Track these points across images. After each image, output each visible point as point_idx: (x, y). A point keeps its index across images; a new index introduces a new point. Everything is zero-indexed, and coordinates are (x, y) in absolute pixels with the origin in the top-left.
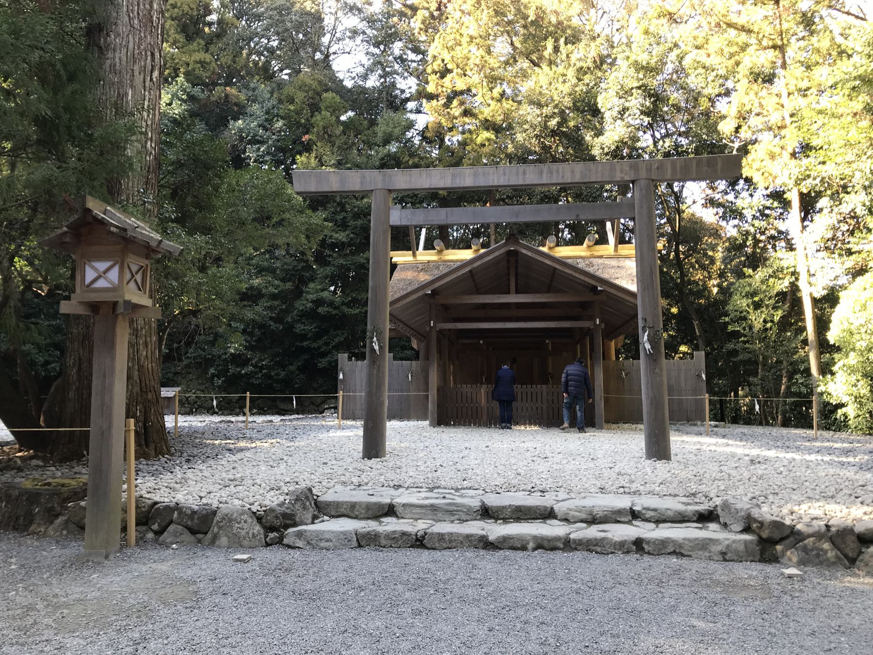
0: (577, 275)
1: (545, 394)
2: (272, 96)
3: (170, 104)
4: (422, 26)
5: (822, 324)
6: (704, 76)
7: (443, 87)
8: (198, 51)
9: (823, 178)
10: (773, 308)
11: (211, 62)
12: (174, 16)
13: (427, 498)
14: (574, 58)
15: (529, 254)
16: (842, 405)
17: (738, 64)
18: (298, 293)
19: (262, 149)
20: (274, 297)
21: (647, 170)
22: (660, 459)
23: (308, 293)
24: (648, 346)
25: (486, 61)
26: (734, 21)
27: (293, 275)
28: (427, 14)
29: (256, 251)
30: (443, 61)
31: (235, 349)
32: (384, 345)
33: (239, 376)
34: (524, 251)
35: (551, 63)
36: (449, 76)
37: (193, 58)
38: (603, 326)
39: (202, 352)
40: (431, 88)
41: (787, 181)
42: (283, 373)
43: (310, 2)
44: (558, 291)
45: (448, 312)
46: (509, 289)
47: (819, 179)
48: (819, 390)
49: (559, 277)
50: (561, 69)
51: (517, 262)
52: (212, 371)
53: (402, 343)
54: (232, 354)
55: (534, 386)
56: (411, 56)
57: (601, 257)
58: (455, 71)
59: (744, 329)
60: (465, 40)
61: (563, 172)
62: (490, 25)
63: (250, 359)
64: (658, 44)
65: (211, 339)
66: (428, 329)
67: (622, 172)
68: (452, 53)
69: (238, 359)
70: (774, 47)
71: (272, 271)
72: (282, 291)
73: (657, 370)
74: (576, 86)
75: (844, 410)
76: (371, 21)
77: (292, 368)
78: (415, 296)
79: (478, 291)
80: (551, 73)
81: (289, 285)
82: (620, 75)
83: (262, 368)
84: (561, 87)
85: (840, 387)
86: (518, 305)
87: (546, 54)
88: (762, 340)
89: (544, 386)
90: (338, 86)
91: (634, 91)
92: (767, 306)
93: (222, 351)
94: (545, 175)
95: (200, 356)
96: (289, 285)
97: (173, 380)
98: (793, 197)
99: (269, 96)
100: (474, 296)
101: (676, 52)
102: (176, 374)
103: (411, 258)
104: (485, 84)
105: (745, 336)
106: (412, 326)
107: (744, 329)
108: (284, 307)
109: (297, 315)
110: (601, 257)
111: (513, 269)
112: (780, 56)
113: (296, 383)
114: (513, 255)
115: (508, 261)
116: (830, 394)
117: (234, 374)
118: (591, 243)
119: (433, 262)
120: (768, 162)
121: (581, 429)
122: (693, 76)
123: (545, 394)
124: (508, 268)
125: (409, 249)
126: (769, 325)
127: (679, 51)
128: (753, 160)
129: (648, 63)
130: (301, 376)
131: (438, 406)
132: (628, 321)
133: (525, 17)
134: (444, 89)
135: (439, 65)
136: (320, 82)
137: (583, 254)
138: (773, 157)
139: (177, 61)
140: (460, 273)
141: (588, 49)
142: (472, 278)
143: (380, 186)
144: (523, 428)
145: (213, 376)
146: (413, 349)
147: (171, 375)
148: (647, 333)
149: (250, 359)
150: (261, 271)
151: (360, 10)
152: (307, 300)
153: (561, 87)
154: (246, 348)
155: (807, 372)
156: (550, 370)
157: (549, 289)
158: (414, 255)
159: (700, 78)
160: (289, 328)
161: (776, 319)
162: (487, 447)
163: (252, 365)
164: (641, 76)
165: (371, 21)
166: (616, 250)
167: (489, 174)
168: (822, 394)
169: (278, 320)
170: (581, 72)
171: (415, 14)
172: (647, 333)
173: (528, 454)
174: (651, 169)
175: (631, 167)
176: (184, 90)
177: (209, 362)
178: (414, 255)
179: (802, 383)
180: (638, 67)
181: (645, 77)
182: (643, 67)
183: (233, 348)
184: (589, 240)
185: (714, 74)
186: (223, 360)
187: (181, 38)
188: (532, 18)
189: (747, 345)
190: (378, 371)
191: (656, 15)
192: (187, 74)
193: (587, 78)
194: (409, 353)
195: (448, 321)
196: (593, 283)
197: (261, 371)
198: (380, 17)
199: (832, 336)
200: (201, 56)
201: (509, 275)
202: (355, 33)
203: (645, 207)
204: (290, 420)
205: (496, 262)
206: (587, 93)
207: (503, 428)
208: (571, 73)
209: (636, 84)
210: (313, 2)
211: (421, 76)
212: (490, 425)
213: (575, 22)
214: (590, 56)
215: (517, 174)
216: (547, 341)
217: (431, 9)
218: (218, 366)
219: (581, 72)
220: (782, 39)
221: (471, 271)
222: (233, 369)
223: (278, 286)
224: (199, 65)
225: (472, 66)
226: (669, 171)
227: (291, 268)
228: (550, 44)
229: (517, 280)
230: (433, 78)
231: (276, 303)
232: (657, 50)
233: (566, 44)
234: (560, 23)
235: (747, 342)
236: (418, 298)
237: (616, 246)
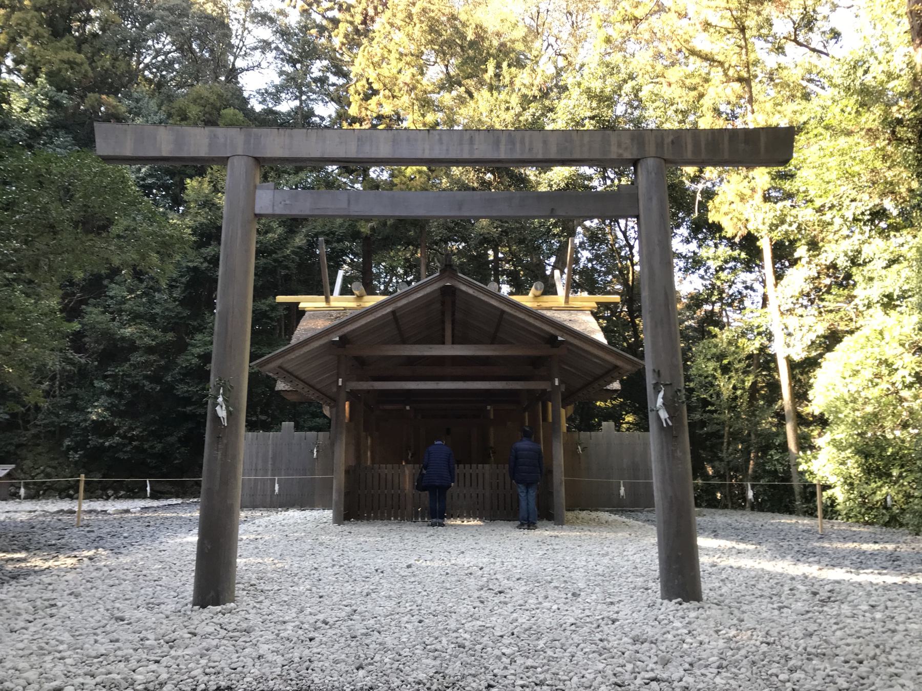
0: (531, 320)
2: (160, 109)
3: (26, 110)
4: (344, 41)
5: (801, 395)
6: (662, 109)
7: (367, 109)
8: (68, 49)
9: (799, 224)
10: (743, 373)
11: (82, 64)
12: (38, 5)
14: (518, 83)
15: (470, 291)
16: (826, 487)
17: (701, 96)
18: (181, 347)
19: (143, 170)
20: (150, 350)
22: (687, 600)
23: (194, 346)
24: (664, 415)
25: (418, 81)
26: (698, 49)
27: (176, 323)
28: (350, 29)
29: (131, 294)
30: (368, 80)
31: (98, 414)
32: (237, 410)
33: (101, 449)
34: (464, 288)
35: (491, 88)
36: (375, 99)
37: (59, 57)
39: (55, 419)
40: (353, 111)
41: (761, 227)
42: (159, 446)
43: (211, 4)
44: (502, 342)
45: (363, 367)
46: (444, 336)
47: (795, 226)
48: (800, 469)
49: (505, 324)
50: (503, 96)
51: (454, 302)
52: (67, 442)
53: (313, 409)
54: (93, 421)
55: (474, 466)
56: (333, 79)
57: (550, 309)
58: (382, 92)
59: (711, 396)
60: (394, 56)
62: (423, 41)
63: (118, 428)
64: (612, 74)
65: (69, 402)
66: (335, 390)
67: (619, 146)
68: (378, 71)
69: (100, 428)
70: (740, 80)
71: (152, 319)
72: (162, 344)
73: (679, 454)
74: (519, 115)
75: (829, 492)
76: (285, 33)
77: (172, 439)
78: (316, 344)
79: (404, 341)
80: (492, 101)
81: (170, 336)
82: (571, 103)
83: (132, 439)
84: (503, 115)
85: (827, 464)
87: (487, 77)
88: (732, 409)
89: (487, 466)
91: (586, 121)
92: (737, 370)
93: (81, 418)
94: (503, 147)
95: (53, 423)
96: (170, 336)
97: (15, 454)
98: (765, 245)
99: (156, 108)
100: (398, 346)
101: (631, 83)
102: (19, 446)
103: (324, 304)
104: (416, 107)
105: (713, 405)
106: (318, 387)
107: (711, 396)
108: (162, 363)
109: (179, 373)
110: (550, 309)
111: (448, 312)
112: (746, 89)
113: (176, 458)
114: (448, 293)
115: (443, 303)
116: (812, 473)
117: (95, 447)
118: (539, 293)
119: (350, 309)
120: (738, 205)
121: (528, 523)
122: (651, 109)
124: (443, 313)
125: (320, 293)
126: (739, 392)
127: (634, 83)
128: (721, 203)
129: (602, 92)
130: (183, 449)
131: (347, 494)
133: (463, 37)
134: (369, 113)
135: (364, 86)
136: (220, 96)
138: (742, 198)
139: (38, 58)
140: (379, 314)
141: (534, 76)
142: (395, 324)
144: (459, 522)
145: (69, 448)
146: (325, 416)
147: (12, 448)
148: (661, 394)
149: (118, 428)
150: (136, 317)
151: (272, 20)
152: (193, 355)
153: (503, 115)
154: (113, 414)
155: (784, 447)
156: (492, 444)
157: (493, 340)
158: (327, 300)
159: (659, 113)
160: (169, 389)
161: (748, 384)
162: (409, 566)
163: (119, 435)
164: (594, 104)
165: (285, 33)
166: (567, 301)
168: (802, 473)
169: (155, 379)
170: (526, 101)
171: (337, 27)
172: (661, 394)
173: (471, 582)
175: (632, 140)
176: (46, 95)
177: (65, 431)
178: (327, 300)
179: (777, 460)
180: (590, 94)
181: (598, 107)
182: (596, 96)
183: (95, 413)
184: (536, 288)
185: (674, 107)
186: (83, 429)
187: (45, 31)
188: (470, 36)
189: (715, 415)
190: (225, 454)
191: (620, 19)
192: (50, 76)
193: (533, 108)
194: (319, 421)
195: (360, 379)
196: (552, 331)
197: (130, 443)
198: (297, 31)
199: (816, 405)
200: (71, 55)
201: (443, 322)
202: (265, 46)
203: (655, 201)
204: (156, 509)
205: (427, 302)
206: (533, 123)
207: (433, 525)
208: (515, 100)
209: (589, 114)
210: (215, 4)
211: (341, 101)
212: (417, 518)
213: (519, 46)
214: (536, 83)
216: (489, 408)
217: (356, 23)
218: (76, 436)
219: (526, 101)
220: (748, 71)
221: (393, 312)
222: (94, 441)
223: (156, 337)
224: (66, 66)
225: (401, 85)
226: (690, 147)
227: (173, 315)
228: (491, 66)
229: (453, 330)
230: (355, 99)
231: (153, 358)
232: (611, 82)
233: (509, 66)
234: (503, 45)
235: (715, 411)
236: (321, 346)
237: (567, 296)
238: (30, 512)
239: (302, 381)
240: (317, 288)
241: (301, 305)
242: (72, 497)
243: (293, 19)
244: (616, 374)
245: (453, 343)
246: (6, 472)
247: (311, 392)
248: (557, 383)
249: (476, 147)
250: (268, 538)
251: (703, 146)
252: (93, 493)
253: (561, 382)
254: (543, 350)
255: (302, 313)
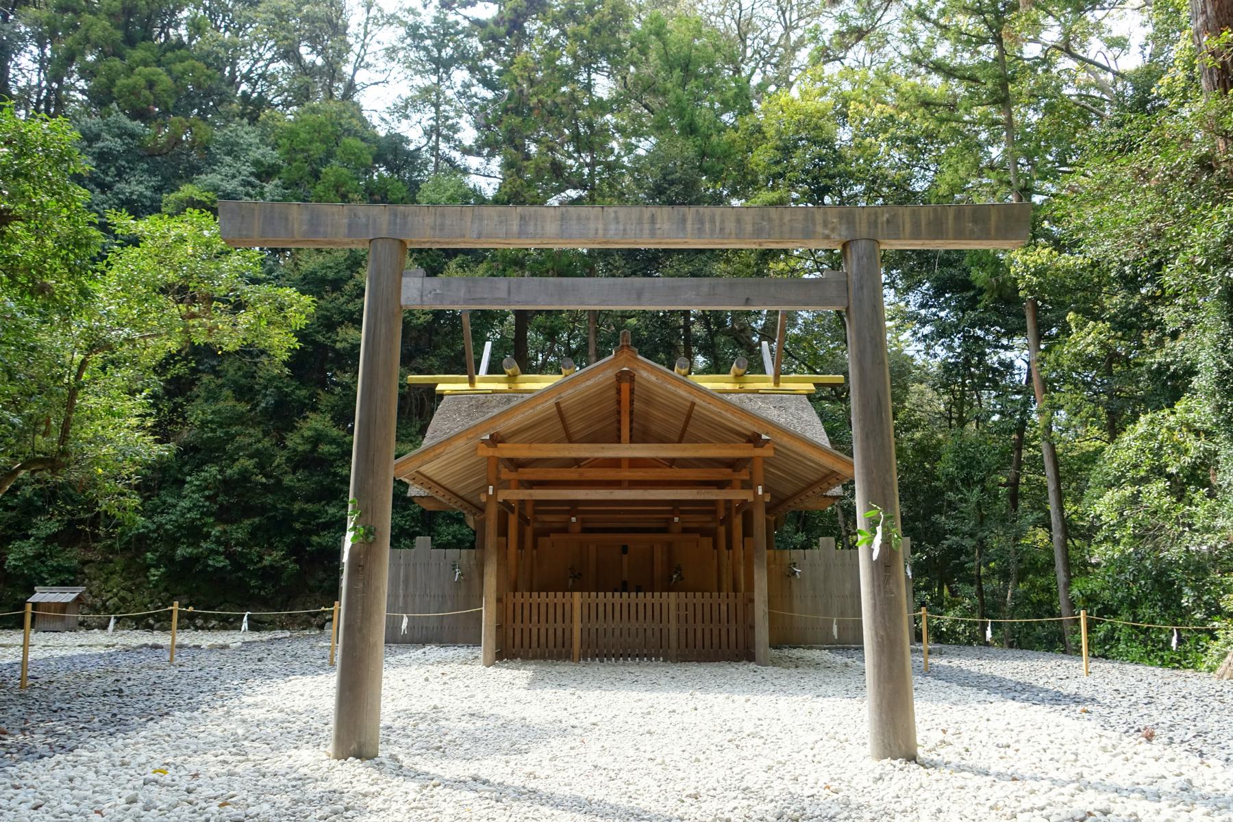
1: (673, 607)
13: (644, 263)
21: (869, 223)
38: (768, 499)
44: (696, 440)
46: (619, 437)
51: (632, 391)
55: (657, 594)
61: (722, 221)
86: (635, 463)
90: (363, 131)
106: (462, 493)
115: (619, 391)
123: (673, 607)
132: (803, 490)
137: (729, 386)
143: (384, 234)
158: (472, 381)
167: (588, 219)
174: (876, 222)
178: (472, 381)
184: (738, 366)
215: (640, 221)
229: (631, 421)
238: (107, 646)
239: (436, 483)
240: (460, 365)
241: (440, 387)
242: (164, 629)
243: (427, 18)
244: (833, 481)
245: (631, 442)
246: (74, 596)
247: (453, 500)
248: (760, 492)
249: (658, 226)
250: (412, 684)
251: (923, 223)
252: (188, 622)
253: (765, 491)
254: (740, 451)
255: (441, 396)
